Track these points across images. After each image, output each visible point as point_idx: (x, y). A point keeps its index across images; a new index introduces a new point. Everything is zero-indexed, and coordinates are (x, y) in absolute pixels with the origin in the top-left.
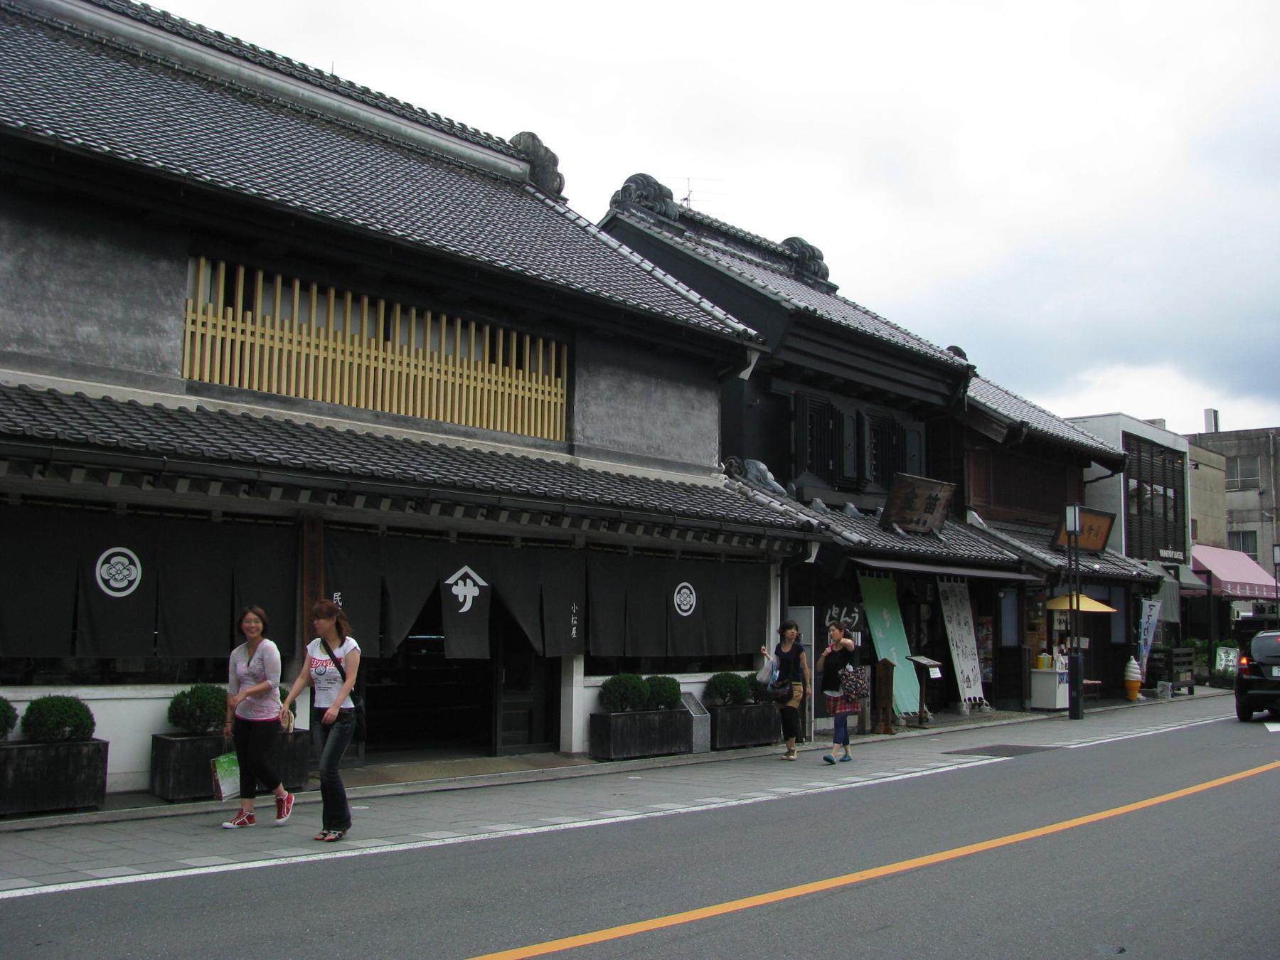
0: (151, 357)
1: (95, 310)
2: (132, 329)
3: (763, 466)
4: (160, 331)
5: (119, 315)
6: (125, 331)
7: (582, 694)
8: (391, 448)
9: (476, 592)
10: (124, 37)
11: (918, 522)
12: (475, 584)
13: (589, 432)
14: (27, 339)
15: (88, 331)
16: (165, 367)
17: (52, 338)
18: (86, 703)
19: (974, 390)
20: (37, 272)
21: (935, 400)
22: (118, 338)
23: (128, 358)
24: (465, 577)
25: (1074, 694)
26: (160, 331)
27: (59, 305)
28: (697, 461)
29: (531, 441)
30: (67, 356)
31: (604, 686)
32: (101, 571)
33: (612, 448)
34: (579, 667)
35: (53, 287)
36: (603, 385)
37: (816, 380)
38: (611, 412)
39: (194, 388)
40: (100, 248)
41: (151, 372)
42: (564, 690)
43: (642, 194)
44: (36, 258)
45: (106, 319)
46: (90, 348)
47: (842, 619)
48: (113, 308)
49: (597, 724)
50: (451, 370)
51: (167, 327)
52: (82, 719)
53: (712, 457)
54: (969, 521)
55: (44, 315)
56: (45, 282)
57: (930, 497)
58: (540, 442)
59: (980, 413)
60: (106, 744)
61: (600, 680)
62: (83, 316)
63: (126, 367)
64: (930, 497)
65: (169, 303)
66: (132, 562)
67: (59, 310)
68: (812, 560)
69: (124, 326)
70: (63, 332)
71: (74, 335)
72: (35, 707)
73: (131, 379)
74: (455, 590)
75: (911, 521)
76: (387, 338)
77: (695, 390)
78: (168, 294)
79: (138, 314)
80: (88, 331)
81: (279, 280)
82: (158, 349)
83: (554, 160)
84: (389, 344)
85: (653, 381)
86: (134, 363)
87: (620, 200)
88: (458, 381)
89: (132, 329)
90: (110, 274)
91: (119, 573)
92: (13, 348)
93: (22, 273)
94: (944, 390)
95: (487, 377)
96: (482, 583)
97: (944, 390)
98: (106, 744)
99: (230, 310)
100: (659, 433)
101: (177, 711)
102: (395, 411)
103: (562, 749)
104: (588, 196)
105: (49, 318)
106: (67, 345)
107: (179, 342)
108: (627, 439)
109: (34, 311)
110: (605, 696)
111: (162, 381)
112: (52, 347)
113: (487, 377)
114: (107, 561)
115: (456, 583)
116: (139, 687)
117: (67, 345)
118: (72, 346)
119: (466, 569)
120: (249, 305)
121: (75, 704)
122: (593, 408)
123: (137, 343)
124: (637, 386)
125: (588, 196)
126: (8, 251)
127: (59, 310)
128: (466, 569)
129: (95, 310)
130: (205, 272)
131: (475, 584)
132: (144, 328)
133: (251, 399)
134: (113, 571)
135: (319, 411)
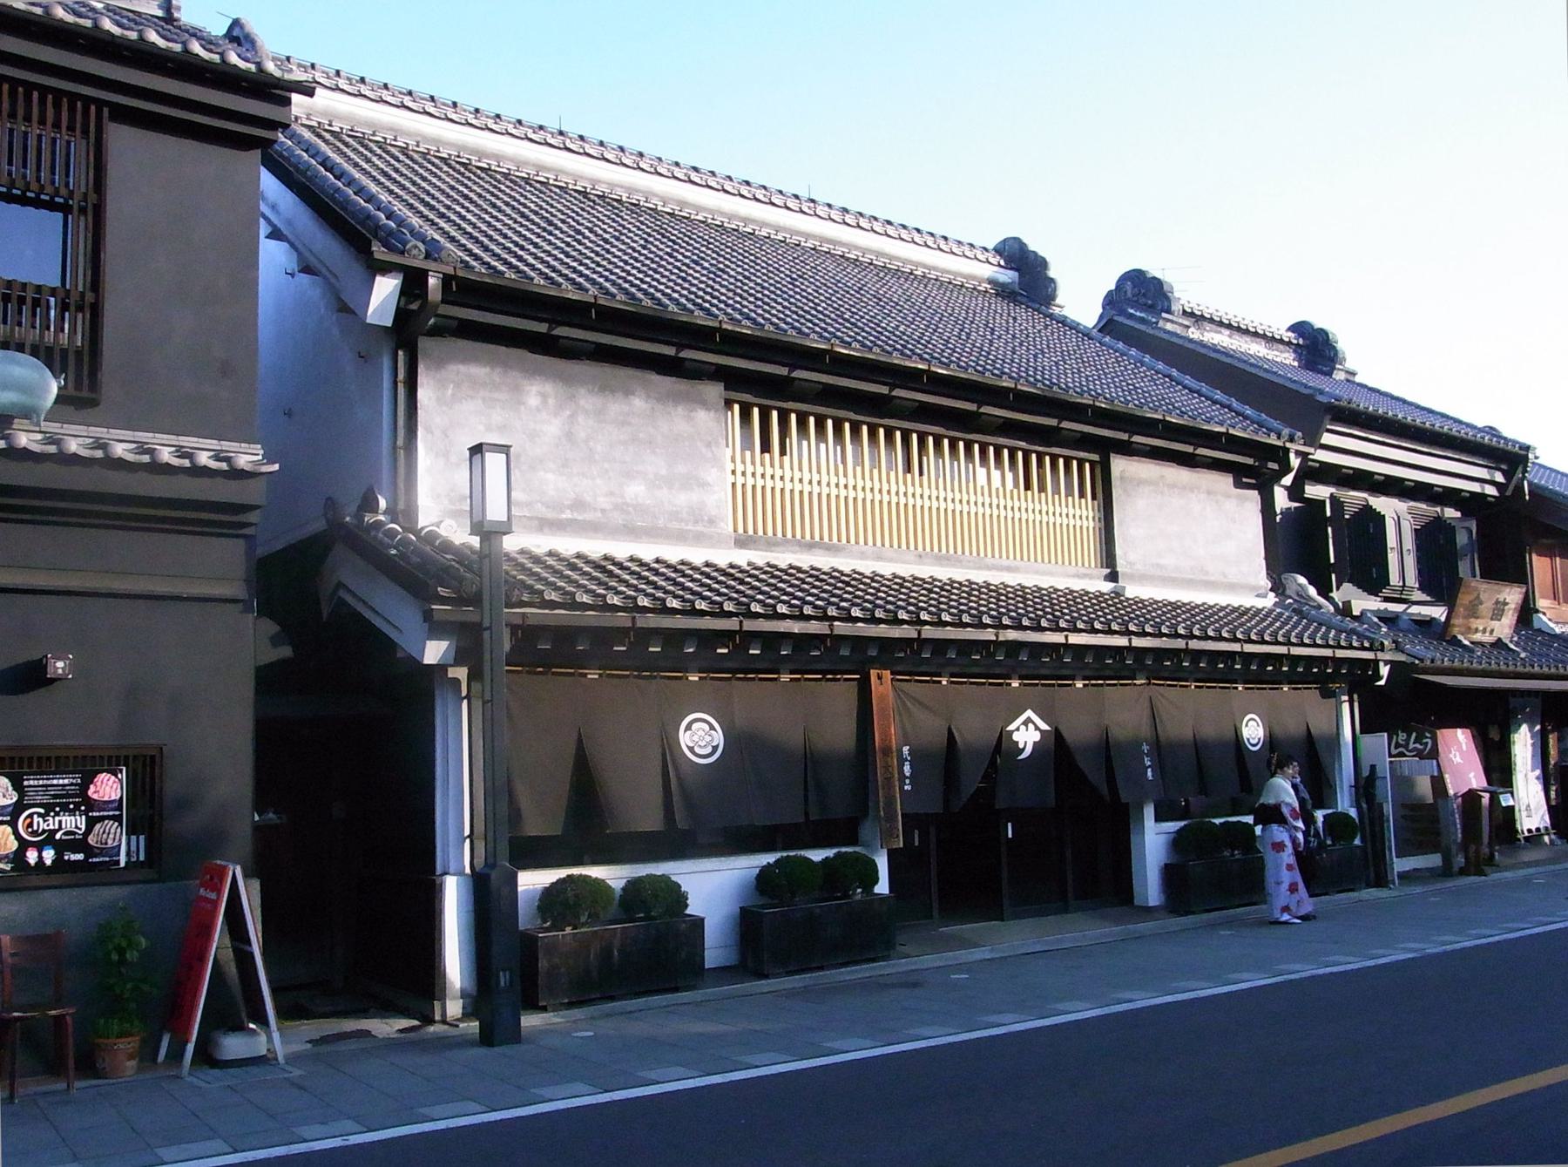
0: (697, 514)
3: (1302, 580)
4: (703, 485)
5: (663, 472)
7: (1154, 840)
8: (818, 579)
9: (1037, 736)
10: (512, 160)
11: (1484, 631)
12: (1037, 728)
17: (603, 502)
19: (1533, 476)
20: (583, 435)
21: (1491, 490)
23: (675, 516)
27: (606, 465)
30: (618, 518)
31: (1179, 831)
34: (1149, 812)
35: (599, 448)
37: (1359, 480)
39: (742, 542)
41: (699, 528)
42: (1133, 838)
43: (1139, 295)
44: (581, 419)
45: (651, 476)
47: (1411, 746)
48: (655, 464)
49: (1172, 875)
50: (842, 481)
51: (709, 479)
52: (675, 897)
54: (1536, 625)
57: (1497, 602)
60: (702, 920)
61: (1173, 826)
62: (629, 475)
63: (675, 525)
64: (1497, 602)
65: (709, 455)
68: (1382, 683)
70: (612, 494)
71: (622, 497)
72: (633, 885)
73: (681, 537)
74: (1016, 737)
75: (1477, 630)
79: (681, 469)
80: (636, 491)
83: (1044, 264)
84: (786, 459)
87: (1112, 301)
88: (950, 506)
92: (567, 515)
94: (1499, 477)
95: (1065, 511)
96: (1045, 727)
97: (1499, 477)
98: (702, 920)
99: (748, 453)
102: (808, 537)
103: (1136, 902)
104: (1081, 298)
105: (598, 481)
108: (1169, 561)
110: (1178, 842)
111: (711, 537)
112: (603, 511)
113: (1078, 513)
114: (688, 728)
118: (621, 508)
119: (1029, 713)
121: (665, 879)
125: (1081, 298)
126: (556, 415)
128: (1029, 713)
131: (1037, 728)
134: (708, 738)
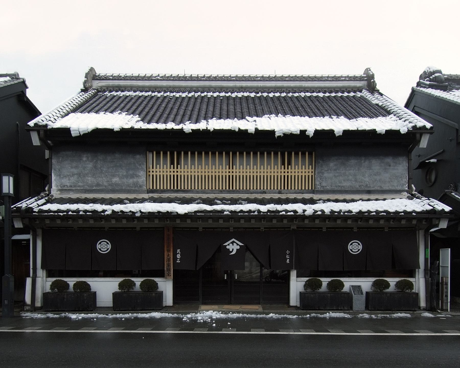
0: (136, 184)
1: (117, 173)
2: (129, 177)
4: (138, 176)
6: (127, 178)
12: (238, 244)
13: (324, 184)
14: (98, 185)
15: (116, 180)
16: (141, 186)
17: (105, 184)
18: (68, 282)
20: (99, 166)
22: (125, 180)
23: (128, 186)
24: (233, 243)
25: (101, 274)
26: (138, 176)
27: (106, 174)
28: (393, 188)
29: (294, 191)
30: (110, 188)
32: (98, 246)
33: (336, 189)
35: (104, 169)
36: (332, 164)
38: (336, 175)
40: (117, 155)
41: (137, 189)
44: (99, 162)
46: (117, 185)
53: (403, 185)
55: (102, 178)
56: (102, 168)
58: (298, 191)
59: (117, 131)
62: (114, 176)
63: (128, 188)
66: (351, 250)
67: (107, 176)
69: (127, 176)
76: (178, 164)
77: (391, 158)
78: (140, 165)
79: (131, 172)
80: (116, 180)
81: (307, 154)
82: (138, 182)
85: (363, 158)
86: (131, 187)
89: (129, 177)
90: (121, 162)
91: (104, 247)
92: (95, 188)
93: (95, 167)
100: (367, 179)
101: (121, 285)
105: (104, 178)
106: (109, 185)
107: (145, 179)
108: (346, 184)
109: (99, 177)
112: (105, 186)
114: (100, 243)
115: (229, 245)
116: (114, 278)
117: (109, 185)
120: (289, 163)
121: (85, 283)
122: (326, 175)
123: (131, 181)
124: (353, 161)
126: (91, 162)
127: (107, 176)
129: (117, 173)
130: (151, 155)
131: (238, 244)
132: (132, 177)
133: (181, 192)
135: (198, 192)
